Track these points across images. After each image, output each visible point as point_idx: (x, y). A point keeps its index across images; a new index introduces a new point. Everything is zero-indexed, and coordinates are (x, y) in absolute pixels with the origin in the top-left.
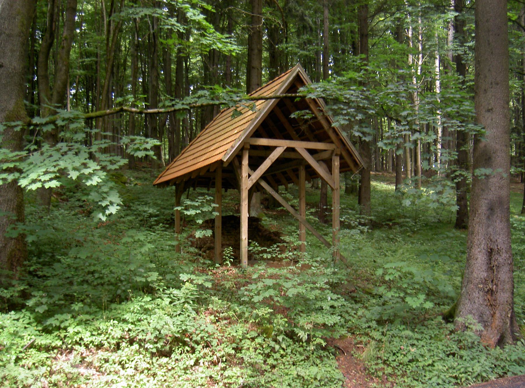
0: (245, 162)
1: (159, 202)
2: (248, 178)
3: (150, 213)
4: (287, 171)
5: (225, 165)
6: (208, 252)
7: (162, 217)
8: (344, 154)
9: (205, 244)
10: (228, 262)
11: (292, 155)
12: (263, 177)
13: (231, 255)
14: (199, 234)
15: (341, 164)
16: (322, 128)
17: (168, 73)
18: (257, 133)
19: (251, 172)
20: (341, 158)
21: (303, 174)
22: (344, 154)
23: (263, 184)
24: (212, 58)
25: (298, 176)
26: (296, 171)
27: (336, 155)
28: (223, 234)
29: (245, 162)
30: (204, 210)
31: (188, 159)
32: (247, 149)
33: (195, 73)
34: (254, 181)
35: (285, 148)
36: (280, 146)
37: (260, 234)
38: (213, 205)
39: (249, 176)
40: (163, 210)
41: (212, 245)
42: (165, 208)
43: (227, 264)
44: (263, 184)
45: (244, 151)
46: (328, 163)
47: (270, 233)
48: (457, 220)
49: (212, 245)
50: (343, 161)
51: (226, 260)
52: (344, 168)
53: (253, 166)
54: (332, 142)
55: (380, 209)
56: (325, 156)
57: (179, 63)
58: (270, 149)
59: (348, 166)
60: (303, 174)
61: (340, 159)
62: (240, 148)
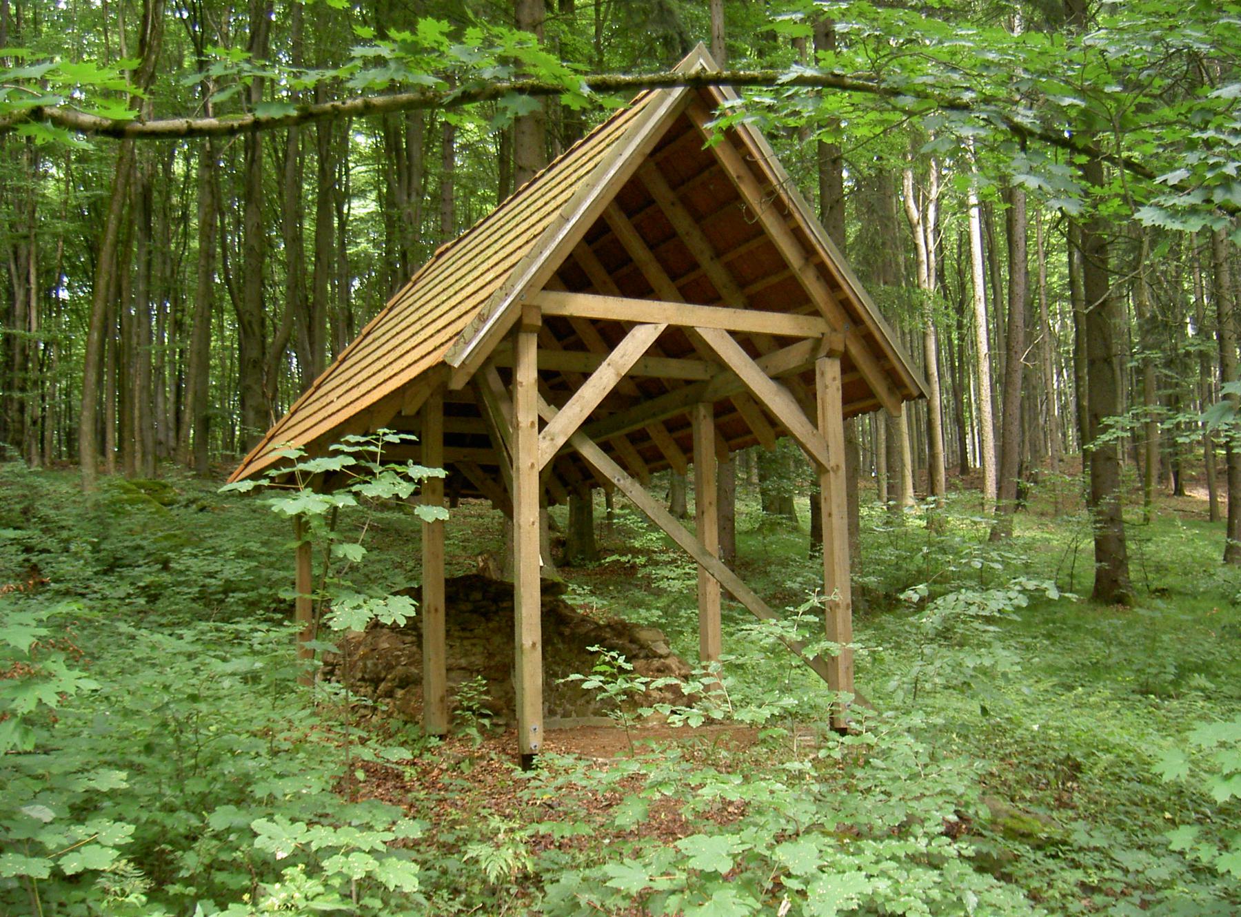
0: (527, 375)
1: (254, 546)
2: (539, 435)
3: (228, 581)
4: (663, 418)
5: (458, 384)
6: (400, 693)
7: (263, 591)
8: (855, 351)
9: (390, 667)
10: (473, 731)
11: (674, 369)
12: (590, 427)
13: (484, 705)
14: (349, 616)
15: (846, 389)
16: (784, 265)
17: (295, 240)
18: (570, 276)
19: (547, 411)
20: (848, 366)
21: (705, 431)
22: (855, 351)
23: (591, 453)
24: (405, 178)
25: (687, 448)
26: (680, 428)
27: (830, 354)
28: (448, 634)
29: (527, 375)
30: (369, 491)
31: (333, 396)
32: (530, 329)
33: (364, 245)
34: (561, 441)
35: (662, 327)
36: (649, 319)
37: (567, 631)
38: (417, 472)
39: (542, 423)
40: (265, 572)
41: (414, 670)
42: (271, 565)
43: (468, 739)
44: (591, 453)
45: (523, 338)
46: (801, 385)
47: (599, 627)
48: (1098, 579)
49: (414, 670)
50: (851, 377)
51: (464, 723)
52: (857, 398)
53: (557, 388)
54: (816, 313)
55: (889, 554)
56: (792, 359)
57: (323, 222)
58: (613, 332)
59: (871, 394)
60: (705, 431)
61: (844, 371)
62: (509, 324)
